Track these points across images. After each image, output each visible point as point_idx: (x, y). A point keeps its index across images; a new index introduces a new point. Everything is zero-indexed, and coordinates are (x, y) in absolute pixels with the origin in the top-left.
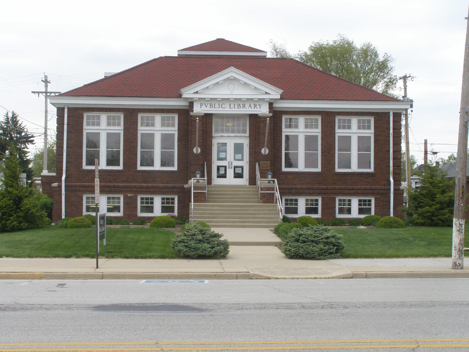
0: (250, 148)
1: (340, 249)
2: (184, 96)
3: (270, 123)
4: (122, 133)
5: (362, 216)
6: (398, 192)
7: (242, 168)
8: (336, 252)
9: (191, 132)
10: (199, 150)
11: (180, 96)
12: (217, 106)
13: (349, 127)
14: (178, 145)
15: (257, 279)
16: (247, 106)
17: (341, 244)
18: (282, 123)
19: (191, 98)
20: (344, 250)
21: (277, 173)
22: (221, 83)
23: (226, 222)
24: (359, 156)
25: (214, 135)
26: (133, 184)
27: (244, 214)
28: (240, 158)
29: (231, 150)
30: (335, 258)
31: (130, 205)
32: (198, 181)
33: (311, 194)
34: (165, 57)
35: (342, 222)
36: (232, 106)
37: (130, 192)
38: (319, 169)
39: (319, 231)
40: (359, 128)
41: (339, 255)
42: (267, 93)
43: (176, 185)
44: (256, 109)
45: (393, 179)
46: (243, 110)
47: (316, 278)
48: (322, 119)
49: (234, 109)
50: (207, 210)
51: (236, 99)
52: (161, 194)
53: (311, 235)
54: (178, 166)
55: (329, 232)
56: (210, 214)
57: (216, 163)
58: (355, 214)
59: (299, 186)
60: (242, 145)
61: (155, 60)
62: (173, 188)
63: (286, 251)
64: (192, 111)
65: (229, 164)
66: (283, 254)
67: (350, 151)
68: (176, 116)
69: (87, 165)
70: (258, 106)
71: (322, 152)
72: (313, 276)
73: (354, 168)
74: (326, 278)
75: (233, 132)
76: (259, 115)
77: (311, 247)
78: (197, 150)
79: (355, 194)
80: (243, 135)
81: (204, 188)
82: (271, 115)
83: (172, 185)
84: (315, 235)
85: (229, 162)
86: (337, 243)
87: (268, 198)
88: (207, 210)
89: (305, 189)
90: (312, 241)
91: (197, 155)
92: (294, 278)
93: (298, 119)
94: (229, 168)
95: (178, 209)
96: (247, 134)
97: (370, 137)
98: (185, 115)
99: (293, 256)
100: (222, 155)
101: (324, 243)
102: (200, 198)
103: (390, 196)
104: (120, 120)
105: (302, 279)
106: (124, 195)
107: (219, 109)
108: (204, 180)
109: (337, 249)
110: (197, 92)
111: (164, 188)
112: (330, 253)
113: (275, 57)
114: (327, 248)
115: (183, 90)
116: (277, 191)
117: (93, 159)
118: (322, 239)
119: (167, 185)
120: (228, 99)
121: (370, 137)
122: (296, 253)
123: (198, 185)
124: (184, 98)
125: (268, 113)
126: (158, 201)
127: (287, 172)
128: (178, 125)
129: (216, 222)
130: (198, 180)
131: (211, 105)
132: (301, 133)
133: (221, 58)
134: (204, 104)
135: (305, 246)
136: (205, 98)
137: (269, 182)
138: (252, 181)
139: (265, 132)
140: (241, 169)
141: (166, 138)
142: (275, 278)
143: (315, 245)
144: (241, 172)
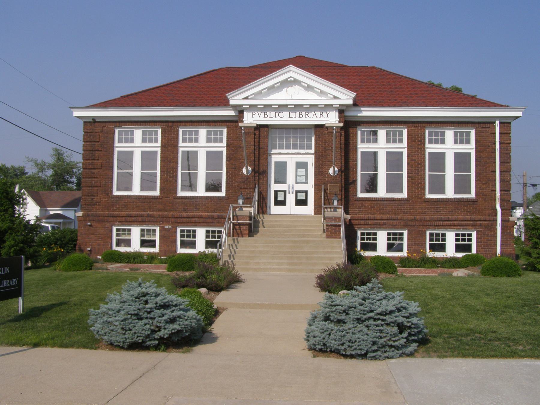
2: (231, 102)
4: (159, 150)
5: (460, 255)
6: (507, 225)
11: (225, 103)
13: (443, 142)
21: (347, 198)
22: (278, 87)
26: (116, 213)
28: (304, 181)
29: (295, 169)
31: (168, 238)
33: (394, 226)
35: (435, 263)
37: (168, 222)
42: (335, 97)
44: (322, 118)
45: (501, 207)
48: (408, 132)
49: (295, 119)
54: (227, 191)
58: (450, 251)
59: (378, 217)
64: (242, 121)
65: (289, 188)
67: (444, 172)
69: (429, 193)
71: (408, 173)
73: (136, 191)
79: (451, 227)
82: (341, 125)
85: (289, 185)
91: (247, 177)
96: (313, 151)
97: (401, 153)
103: (496, 229)
106: (160, 227)
110: (247, 98)
115: (229, 95)
120: (286, 106)
121: (222, 152)
125: (337, 122)
126: (382, 237)
128: (227, 141)
132: (381, 147)
136: (302, 105)
138: (318, 210)
139: (338, 145)
140: (304, 194)
144: (304, 198)
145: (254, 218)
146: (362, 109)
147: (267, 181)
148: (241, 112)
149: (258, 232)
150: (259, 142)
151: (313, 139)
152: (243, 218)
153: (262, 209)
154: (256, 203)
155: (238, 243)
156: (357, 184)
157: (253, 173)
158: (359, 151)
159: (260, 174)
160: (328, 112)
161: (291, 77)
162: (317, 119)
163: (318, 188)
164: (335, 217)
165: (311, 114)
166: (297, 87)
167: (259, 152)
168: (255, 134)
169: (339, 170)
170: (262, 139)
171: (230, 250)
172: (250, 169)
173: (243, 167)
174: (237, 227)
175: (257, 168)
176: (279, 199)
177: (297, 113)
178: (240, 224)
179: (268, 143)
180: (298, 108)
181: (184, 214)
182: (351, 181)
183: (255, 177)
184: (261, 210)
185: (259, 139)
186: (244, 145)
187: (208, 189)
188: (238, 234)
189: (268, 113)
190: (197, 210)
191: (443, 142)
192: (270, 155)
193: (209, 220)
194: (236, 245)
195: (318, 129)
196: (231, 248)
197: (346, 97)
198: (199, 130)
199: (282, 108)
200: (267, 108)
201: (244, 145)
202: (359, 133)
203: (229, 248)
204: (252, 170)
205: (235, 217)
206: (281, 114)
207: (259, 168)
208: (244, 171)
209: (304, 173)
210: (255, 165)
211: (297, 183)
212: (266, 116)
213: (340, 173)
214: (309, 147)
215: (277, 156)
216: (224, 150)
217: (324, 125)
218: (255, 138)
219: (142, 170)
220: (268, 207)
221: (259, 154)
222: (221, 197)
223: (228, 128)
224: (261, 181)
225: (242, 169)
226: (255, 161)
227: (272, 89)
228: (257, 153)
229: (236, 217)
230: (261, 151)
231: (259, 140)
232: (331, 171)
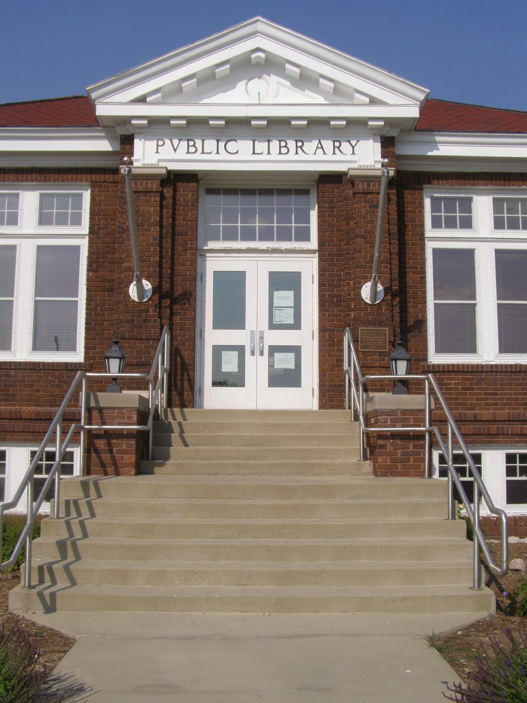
0: (321, 285)
2: (101, 110)
7: (296, 350)
14: (89, 280)
28: (291, 321)
42: (373, 101)
46: (297, 158)
49: (269, 158)
59: (486, 414)
65: (252, 341)
85: (252, 333)
91: (139, 308)
96: (314, 243)
107: (218, 157)
110: (142, 100)
121: (77, 248)
128: (92, 219)
138: (332, 393)
144: (291, 366)
145: (156, 416)
146: (438, 139)
147: (193, 320)
148: (127, 142)
149: (167, 457)
150: (174, 219)
151: (314, 215)
152: (119, 413)
153: (181, 395)
154: (162, 375)
155: (99, 496)
156: (426, 331)
157: (156, 297)
158: (430, 246)
159: (174, 301)
160: (353, 142)
161: (258, 50)
162: (325, 158)
163: (331, 338)
164: (405, 412)
165: (310, 146)
166: (274, 79)
167: (173, 243)
168: (162, 197)
169: (385, 289)
170: (180, 209)
171: (68, 524)
172: (147, 285)
173: (131, 282)
174: (101, 444)
175: (166, 286)
177: (275, 144)
178: (108, 435)
179: (196, 220)
180: (277, 127)
182: (411, 321)
183: (160, 308)
184: (176, 398)
185: (174, 209)
186: (131, 223)
188: (103, 465)
189: (199, 143)
191: (467, 223)
192: (203, 254)
194: (89, 504)
195: (328, 187)
196: (74, 514)
198: (21, 193)
199: (236, 127)
200: (196, 127)
201: (131, 223)
202: (427, 203)
203: (68, 513)
204: (155, 290)
205: (95, 413)
206: (232, 146)
207: (172, 284)
208: (133, 292)
209: (291, 302)
210: (161, 277)
211: (272, 326)
212: (192, 149)
213: (389, 297)
214: (304, 235)
216: (84, 244)
217: (345, 174)
218: (161, 207)
219: (36, 296)
220: (196, 389)
221: (173, 249)
222: (71, 364)
223: (94, 186)
224: (177, 319)
225: (128, 287)
226: (161, 267)
227: (209, 81)
228: (167, 245)
229: (95, 412)
230: (180, 240)
231: (174, 214)
232: (366, 292)
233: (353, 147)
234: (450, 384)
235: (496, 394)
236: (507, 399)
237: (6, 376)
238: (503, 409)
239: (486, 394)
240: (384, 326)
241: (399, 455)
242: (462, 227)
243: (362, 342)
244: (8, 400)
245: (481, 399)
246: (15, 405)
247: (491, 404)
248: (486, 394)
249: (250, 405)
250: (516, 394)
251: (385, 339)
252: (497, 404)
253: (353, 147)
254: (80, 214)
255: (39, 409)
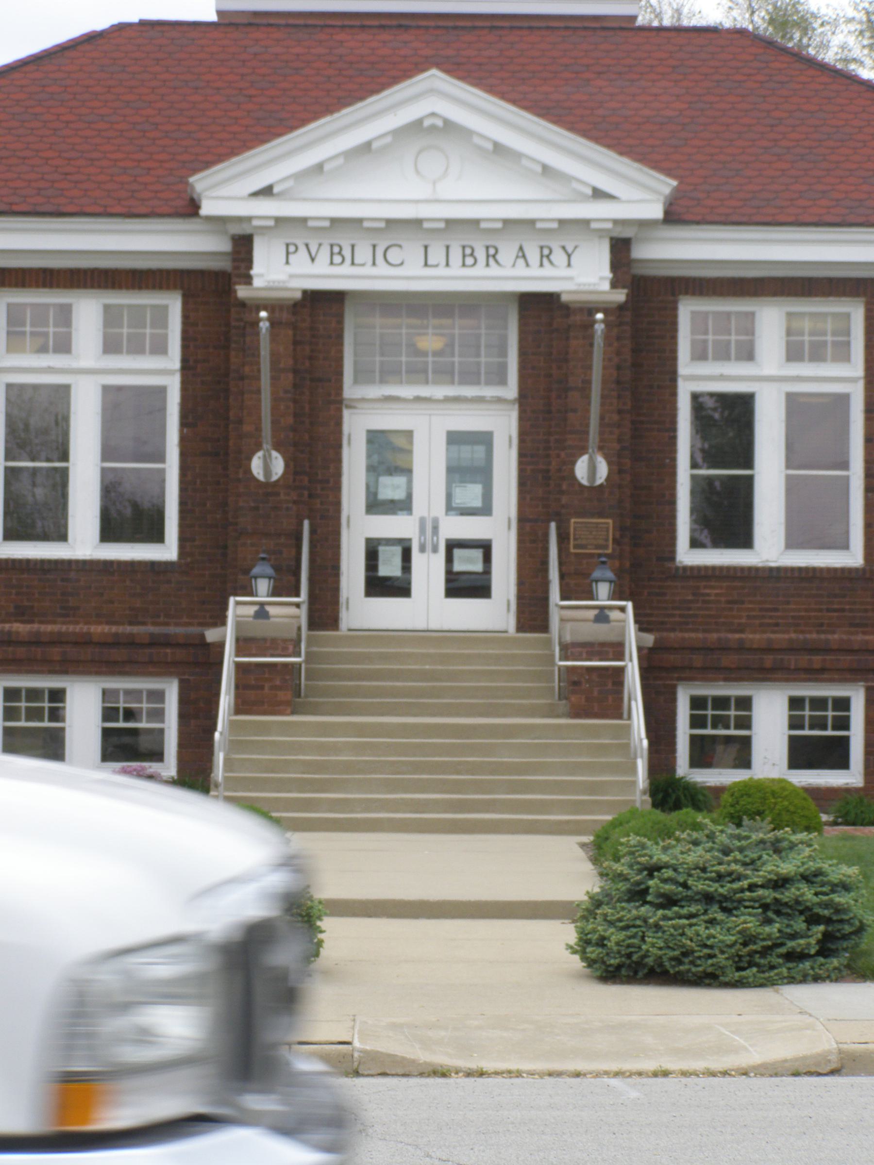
0: (522, 455)
1: (845, 937)
2: (208, 208)
3: (607, 337)
7: (486, 547)
8: (825, 951)
9: (242, 378)
10: (278, 466)
11: (190, 208)
12: (363, 254)
14: (183, 440)
15: (384, 1074)
16: (507, 254)
17: (846, 911)
18: (674, 338)
19: (240, 220)
20: (866, 942)
21: (645, 573)
23: (384, 805)
24: (792, 487)
25: (350, 390)
27: (473, 768)
28: (478, 503)
29: (432, 466)
30: (817, 979)
32: (262, 613)
34: (143, 23)
36: (437, 255)
38: (853, 557)
39: (741, 850)
40: (794, 354)
41: (835, 962)
42: (599, 194)
43: (172, 630)
44: (548, 271)
47: (666, 1074)
50: (300, 748)
51: (451, 224)
52: (98, 673)
53: (704, 870)
54: (183, 540)
55: (792, 855)
56: (308, 766)
57: (358, 527)
60: (485, 439)
61: (91, 38)
62: (155, 642)
63: (588, 942)
64: (248, 279)
66: (577, 957)
68: (174, 305)
70: (559, 257)
72: (650, 1065)
74: (713, 1074)
75: (445, 374)
76: (564, 298)
77: (701, 929)
78: (268, 465)
80: (489, 392)
81: (292, 645)
82: (620, 296)
83: (151, 629)
84: (722, 868)
85: (422, 522)
86: (826, 905)
87: (592, 694)
88: (300, 748)
89: (30, 643)
90: (708, 898)
91: (269, 489)
92: (559, 1074)
93: (753, 314)
94: (422, 549)
95: (181, 745)
96: (511, 390)
97: (843, 400)
98: (213, 295)
99: (619, 967)
100: (391, 488)
101: (765, 907)
102: (268, 690)
104: (165, 325)
105: (598, 1075)
107: (374, 271)
108: (298, 605)
109: (827, 937)
110: (267, 192)
111: (116, 642)
112: (792, 957)
113: (744, 23)
114: (773, 929)
116: (631, 660)
117: (728, 515)
118: (752, 887)
119: (128, 629)
120: (416, 224)
121: (161, 391)
122: (629, 956)
123: (261, 629)
124: (210, 219)
125: (606, 286)
126: (770, 719)
127: (699, 568)
129: (335, 806)
130: (262, 604)
131: (336, 251)
133: (407, 28)
134: (302, 249)
135: (671, 921)
137: (602, 616)
138: (532, 612)
139: (599, 380)
140: (478, 554)
141: (126, 408)
142: (469, 1074)
143: (720, 916)
144: (478, 567)
161: (433, 114)
164: (603, 644)
173: (253, 453)
176: (384, 571)
181: (20, 628)
187: (110, 531)
190: (68, 613)
193: (117, 654)
197: (637, 194)
211: (450, 508)
215: (367, 413)
225: (250, 459)
233: (569, 256)
234: (708, 595)
235: (776, 610)
236: (793, 617)
237: (63, 580)
238: (788, 632)
239: (761, 610)
240: (607, 517)
241: (596, 694)
242: (739, 358)
243: (575, 539)
244: (67, 616)
245: (755, 617)
246: (77, 623)
247: (769, 625)
248: (761, 610)
249: (420, 624)
250: (806, 610)
251: (608, 535)
252: (777, 625)
253: (569, 256)
254: (165, 337)
255: (114, 629)
